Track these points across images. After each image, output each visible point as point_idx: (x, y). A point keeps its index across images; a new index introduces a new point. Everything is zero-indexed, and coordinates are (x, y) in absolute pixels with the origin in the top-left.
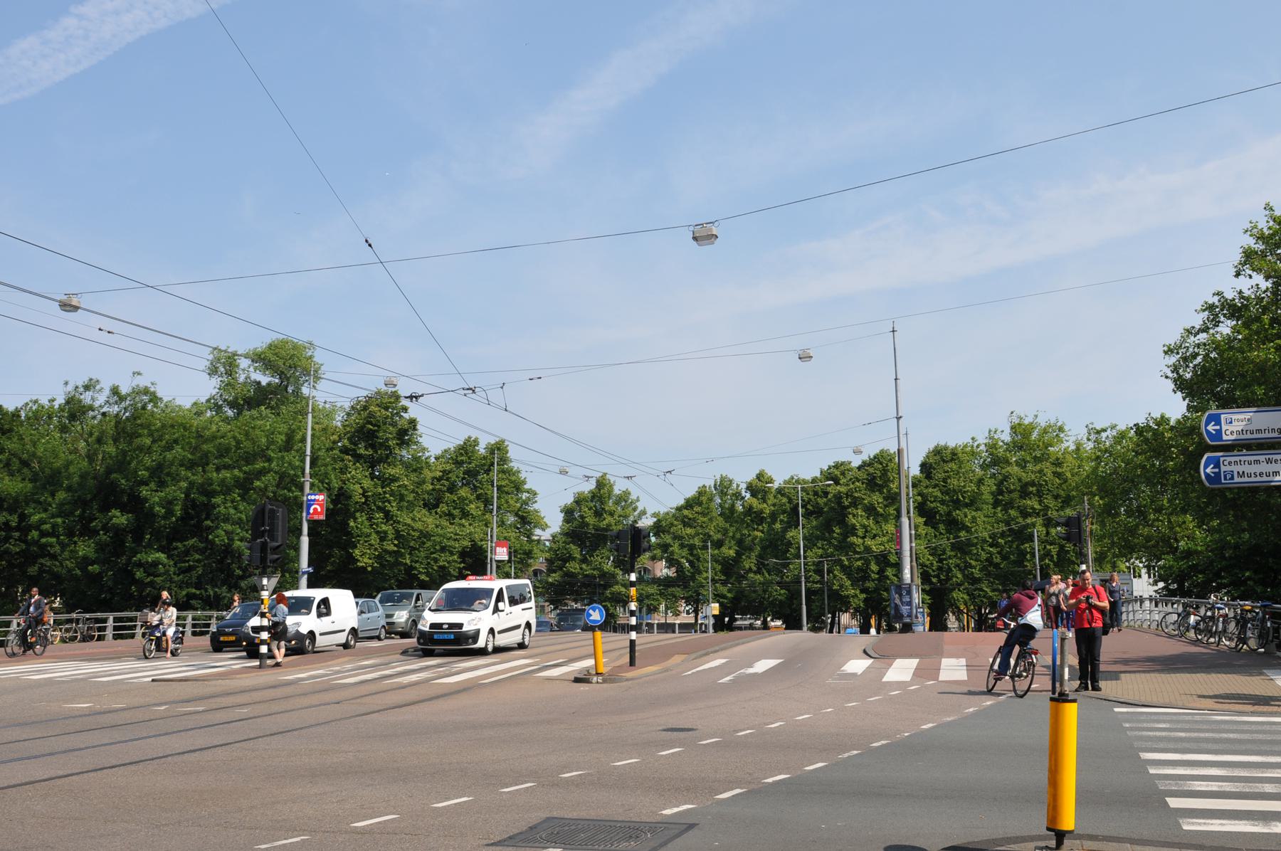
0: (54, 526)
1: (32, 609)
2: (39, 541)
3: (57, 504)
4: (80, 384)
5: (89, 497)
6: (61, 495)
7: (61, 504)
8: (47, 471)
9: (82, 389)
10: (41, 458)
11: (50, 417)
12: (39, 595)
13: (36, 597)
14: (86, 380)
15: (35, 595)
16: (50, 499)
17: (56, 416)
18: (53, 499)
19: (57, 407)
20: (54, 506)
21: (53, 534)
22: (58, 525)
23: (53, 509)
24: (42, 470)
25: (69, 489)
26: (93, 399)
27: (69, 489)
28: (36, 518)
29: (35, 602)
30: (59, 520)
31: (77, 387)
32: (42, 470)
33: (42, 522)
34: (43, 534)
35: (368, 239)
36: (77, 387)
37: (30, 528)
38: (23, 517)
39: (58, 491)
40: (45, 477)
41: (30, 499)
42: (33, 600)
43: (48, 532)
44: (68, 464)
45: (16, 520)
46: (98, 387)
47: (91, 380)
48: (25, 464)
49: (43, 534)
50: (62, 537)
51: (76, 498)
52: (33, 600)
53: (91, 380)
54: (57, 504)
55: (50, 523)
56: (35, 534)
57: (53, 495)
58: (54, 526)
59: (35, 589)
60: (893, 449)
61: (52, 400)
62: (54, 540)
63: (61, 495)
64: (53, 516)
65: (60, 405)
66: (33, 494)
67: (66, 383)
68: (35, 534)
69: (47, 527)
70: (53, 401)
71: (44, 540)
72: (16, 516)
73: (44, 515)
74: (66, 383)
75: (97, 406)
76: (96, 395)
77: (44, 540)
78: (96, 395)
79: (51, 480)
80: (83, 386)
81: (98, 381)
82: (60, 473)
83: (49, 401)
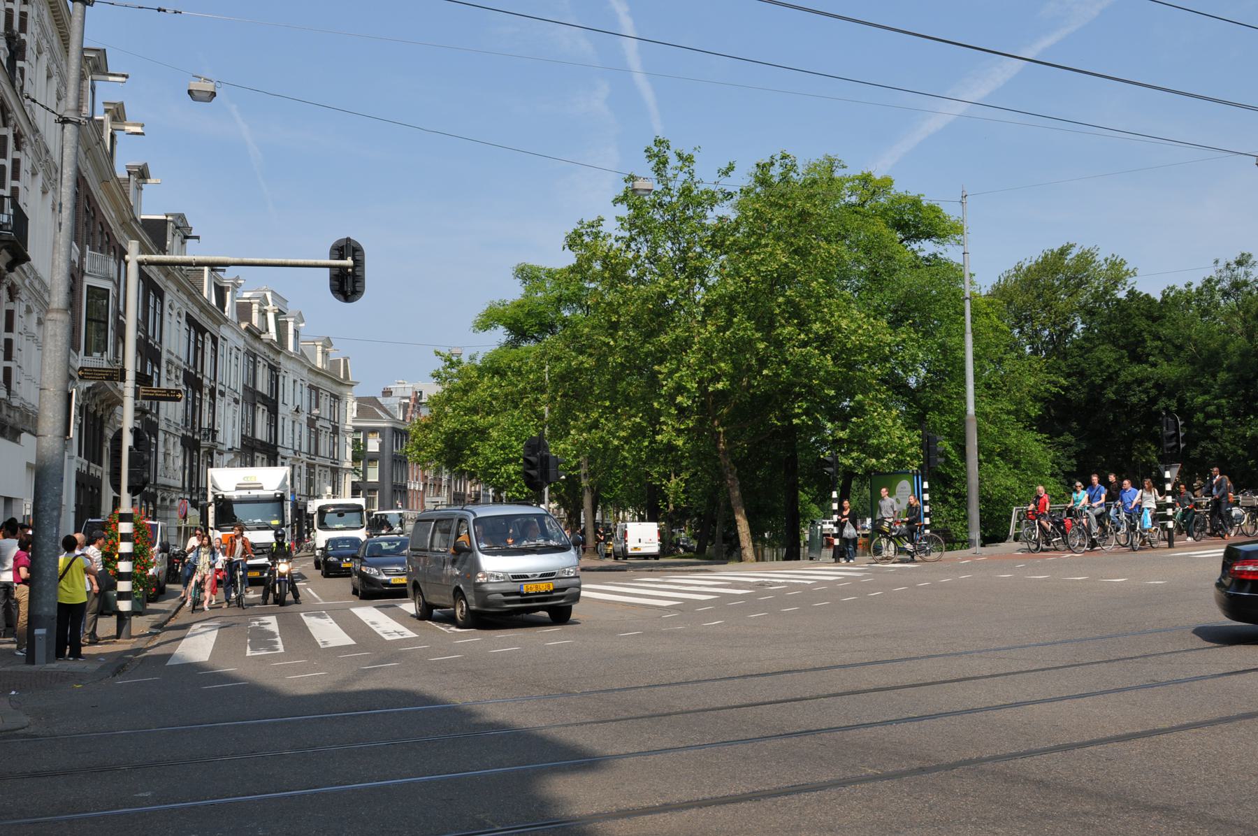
0: (1219, 407)
1: (1214, 490)
2: (1205, 423)
3: (1220, 385)
4: (1232, 260)
5: (1252, 375)
6: (1223, 376)
7: (1224, 385)
8: (1205, 353)
9: (1235, 266)
10: (1196, 340)
11: (1189, 302)
12: (1221, 475)
13: (1217, 477)
14: (1238, 255)
15: (1216, 475)
16: (1211, 381)
17: (1195, 300)
18: (1215, 380)
19: (1194, 291)
20: (1216, 387)
21: (1219, 414)
22: (1222, 406)
23: (1216, 389)
24: (1199, 352)
25: (1229, 369)
26: (1246, 274)
27: (1229, 369)
28: (1200, 399)
29: (1216, 483)
30: (1223, 401)
31: (1228, 264)
32: (1199, 352)
33: (1206, 404)
34: (1208, 416)
35: (196, 85)
36: (1228, 264)
37: (1193, 411)
38: (1181, 402)
39: (1218, 372)
40: (1204, 359)
41: (1191, 382)
42: (1215, 481)
43: (1214, 414)
44: (1224, 345)
45: (1176, 405)
46: (1251, 261)
47: (1243, 255)
48: (1180, 348)
49: (1208, 416)
50: (1228, 418)
51: (1238, 378)
52: (1215, 481)
53: (1243, 255)
54: (1220, 385)
55: (1215, 405)
56: (1200, 416)
57: (1214, 376)
58: (1219, 407)
59: (1215, 469)
60: (962, 263)
61: (1189, 285)
62: (1220, 421)
63: (1223, 376)
64: (1216, 397)
65: (1197, 289)
66: (1193, 377)
67: (1217, 262)
68: (1200, 416)
69: (1212, 408)
70: (1190, 285)
71: (1209, 422)
72: (1175, 401)
73: (1207, 397)
74: (1217, 262)
75: (1251, 281)
76: (1250, 270)
77: (1209, 422)
78: (1250, 270)
79: (1209, 362)
80: (1236, 262)
81: (1250, 255)
82: (1218, 353)
83: (1186, 286)
